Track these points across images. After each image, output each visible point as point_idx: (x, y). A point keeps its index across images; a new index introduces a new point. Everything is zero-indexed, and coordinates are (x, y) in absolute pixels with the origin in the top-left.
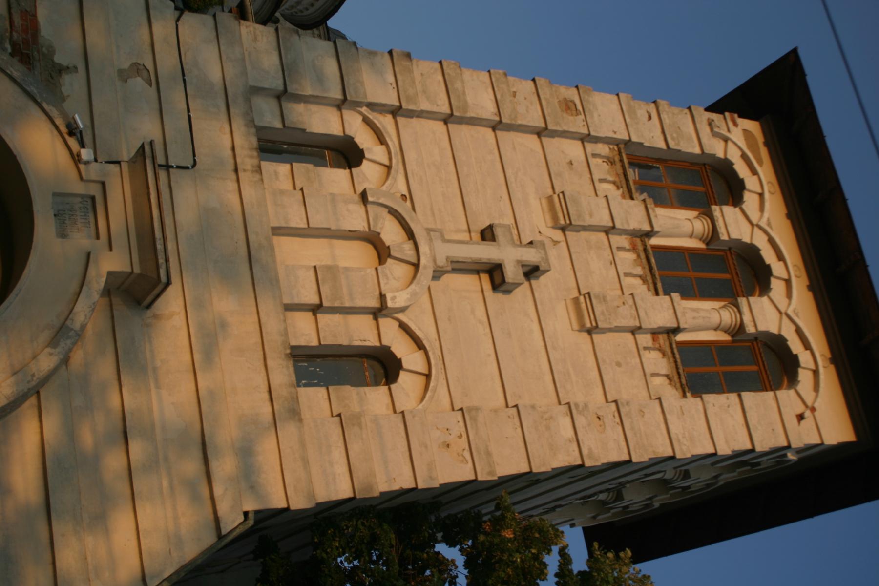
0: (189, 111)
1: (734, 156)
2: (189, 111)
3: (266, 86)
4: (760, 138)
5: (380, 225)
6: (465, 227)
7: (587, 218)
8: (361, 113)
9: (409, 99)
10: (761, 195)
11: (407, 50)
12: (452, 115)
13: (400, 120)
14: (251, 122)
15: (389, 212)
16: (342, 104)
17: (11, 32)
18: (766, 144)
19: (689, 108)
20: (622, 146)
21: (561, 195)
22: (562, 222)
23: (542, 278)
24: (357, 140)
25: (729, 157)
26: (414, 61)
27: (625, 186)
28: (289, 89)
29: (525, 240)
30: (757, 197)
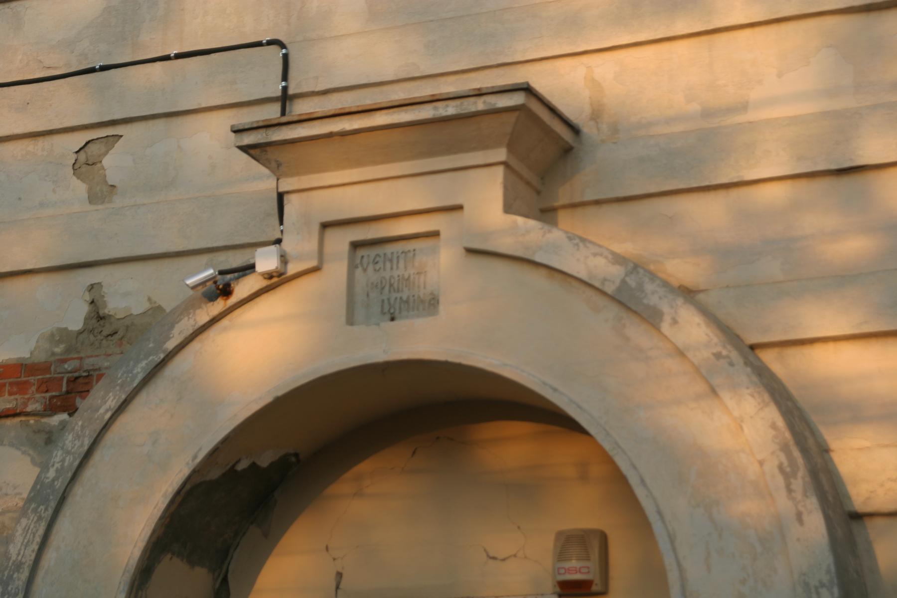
0: (166, 58)
2: (166, 58)
17: (28, 414)
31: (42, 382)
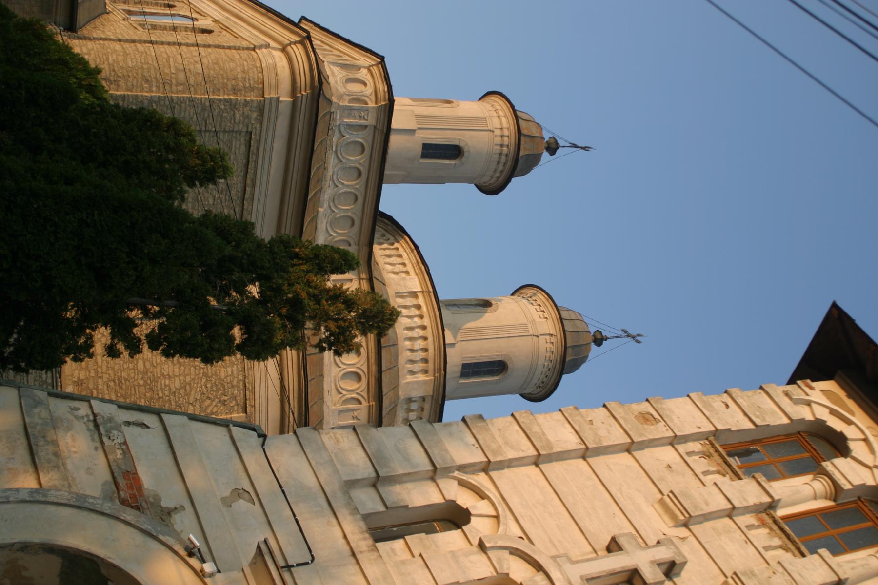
0: (294, 515)
1: (823, 414)
2: (294, 515)
3: (359, 477)
4: (842, 394)
5: (505, 566)
6: (590, 549)
7: (704, 507)
8: (454, 478)
9: (495, 453)
10: (866, 440)
11: (478, 413)
12: (539, 455)
13: (493, 474)
14: (355, 511)
15: (511, 553)
16: (435, 473)
17: (118, 492)
18: (849, 396)
19: (761, 388)
20: (712, 438)
21: (671, 495)
22: (682, 518)
23: (683, 573)
24: (459, 502)
25: (818, 417)
26: (488, 421)
27: (730, 472)
28: (381, 474)
29: (652, 541)
30: (862, 443)
31: (134, 496)
